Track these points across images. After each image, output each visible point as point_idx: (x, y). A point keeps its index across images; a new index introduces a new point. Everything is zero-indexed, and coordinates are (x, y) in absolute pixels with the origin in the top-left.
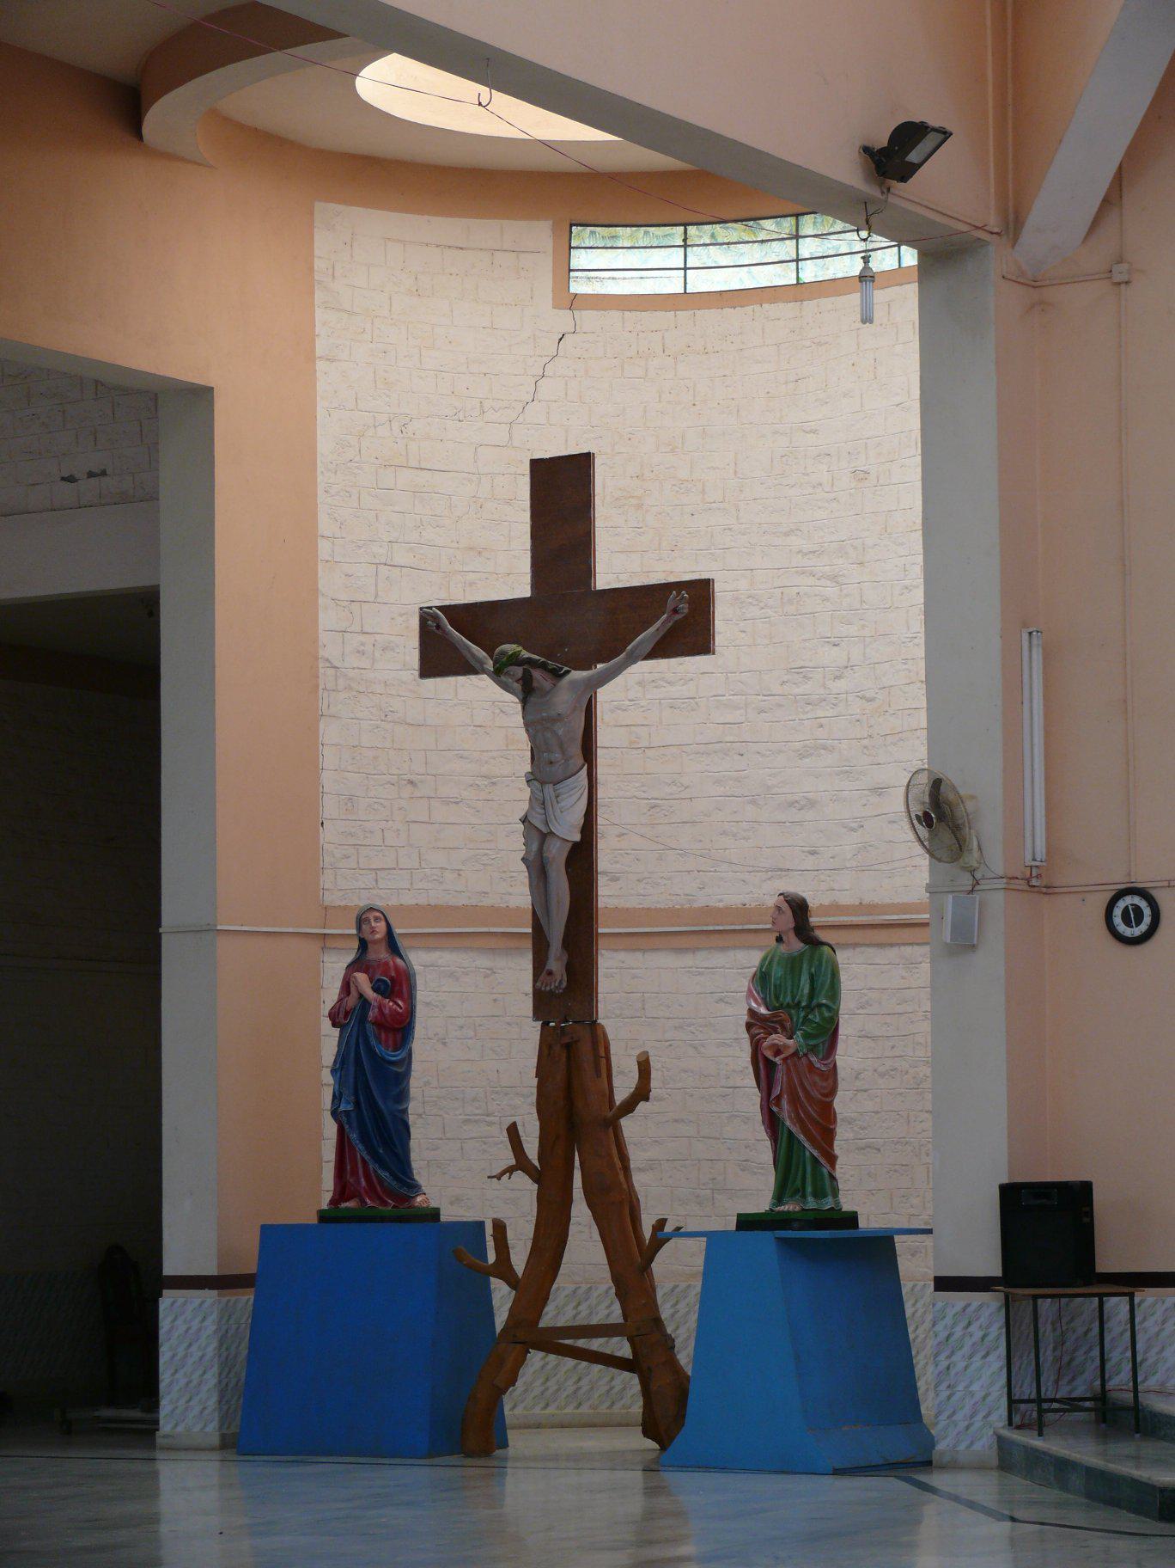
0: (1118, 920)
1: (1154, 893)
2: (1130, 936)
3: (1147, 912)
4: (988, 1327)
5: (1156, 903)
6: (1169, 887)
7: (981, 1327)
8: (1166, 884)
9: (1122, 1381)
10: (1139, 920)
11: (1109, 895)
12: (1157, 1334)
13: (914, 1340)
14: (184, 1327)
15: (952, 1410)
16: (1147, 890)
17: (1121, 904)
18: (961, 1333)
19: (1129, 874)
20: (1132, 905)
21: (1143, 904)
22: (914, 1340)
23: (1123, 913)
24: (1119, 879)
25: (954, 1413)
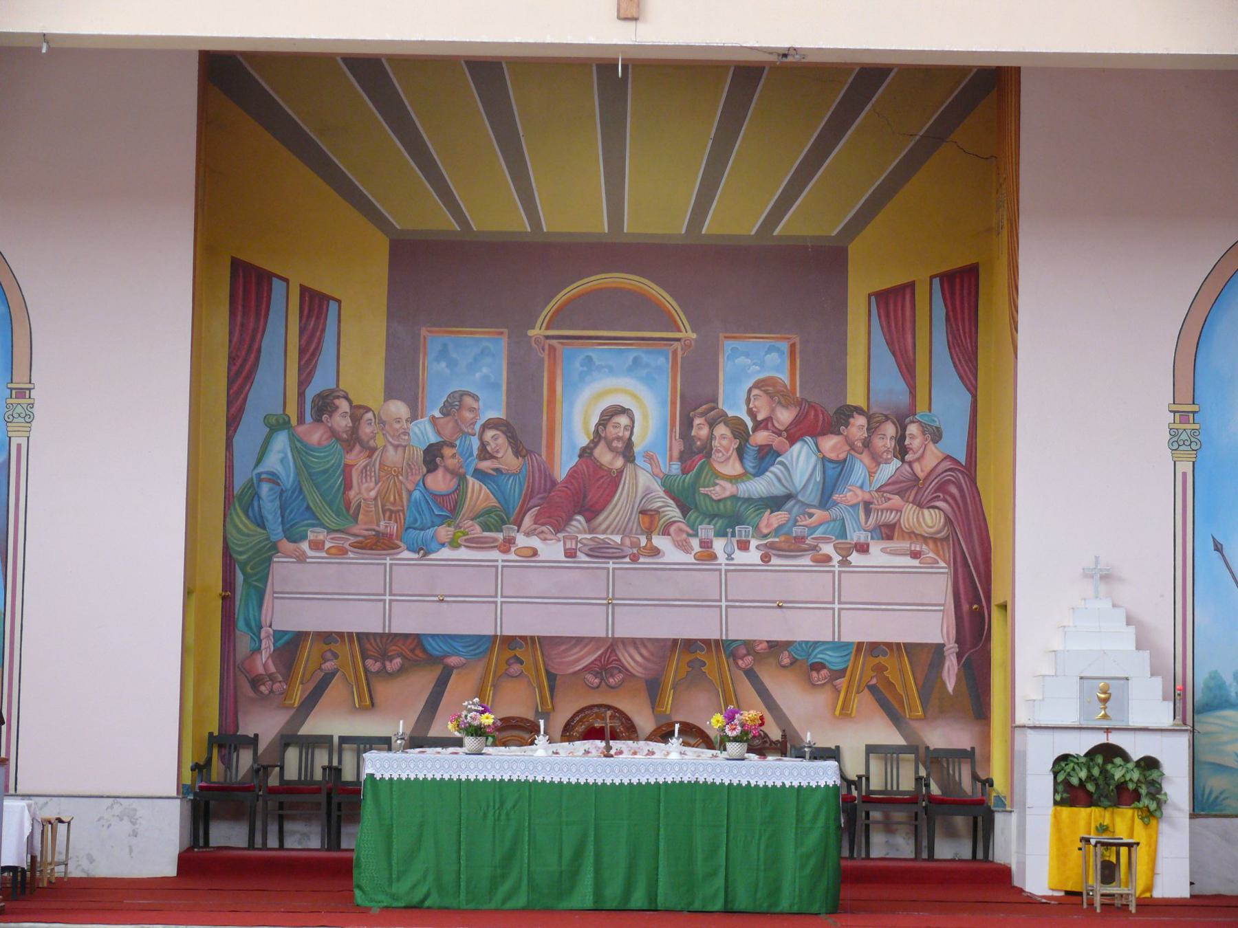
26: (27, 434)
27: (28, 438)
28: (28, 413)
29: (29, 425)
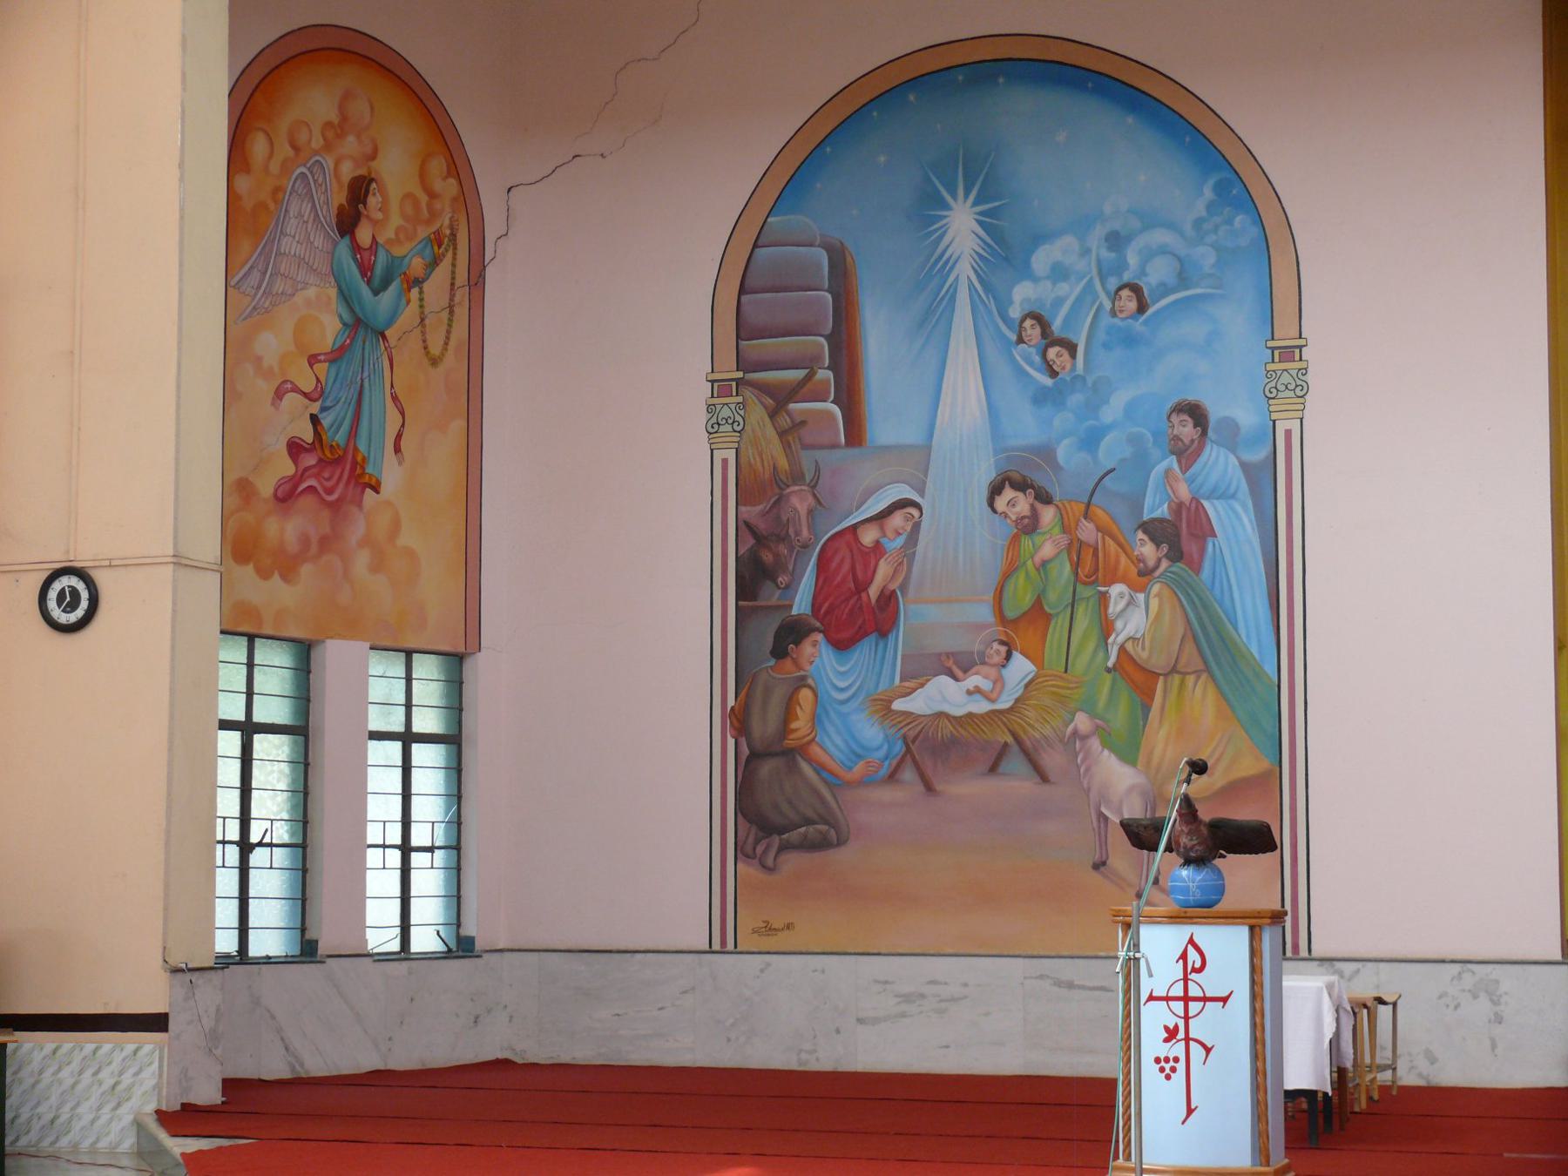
0: (52, 604)
1: (96, 575)
2: (60, 578)
3: (84, 595)
4: (111, 1119)
5: (96, 590)
6: (110, 566)
7: (39, 1118)
8: (107, 563)
9: (30, 1142)
10: (73, 606)
11: (45, 575)
12: (73, 1086)
13: (13, 1121)
14: (121, 1111)
15: (15, 1136)
16: (86, 570)
17: (57, 586)
18: (108, 1116)
19: (68, 552)
20: (69, 587)
21: (81, 586)
22: (13, 1121)
23: (58, 595)
24: (58, 559)
25: (78, 1104)
26: (1299, 414)
27: (1302, 419)
28: (1299, 382)
29: (1301, 400)
